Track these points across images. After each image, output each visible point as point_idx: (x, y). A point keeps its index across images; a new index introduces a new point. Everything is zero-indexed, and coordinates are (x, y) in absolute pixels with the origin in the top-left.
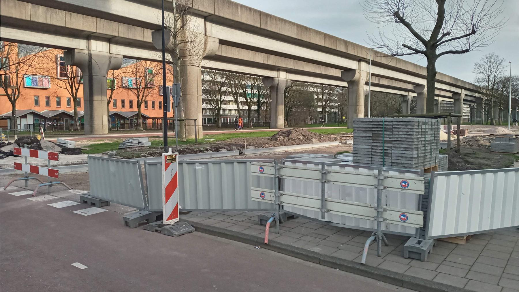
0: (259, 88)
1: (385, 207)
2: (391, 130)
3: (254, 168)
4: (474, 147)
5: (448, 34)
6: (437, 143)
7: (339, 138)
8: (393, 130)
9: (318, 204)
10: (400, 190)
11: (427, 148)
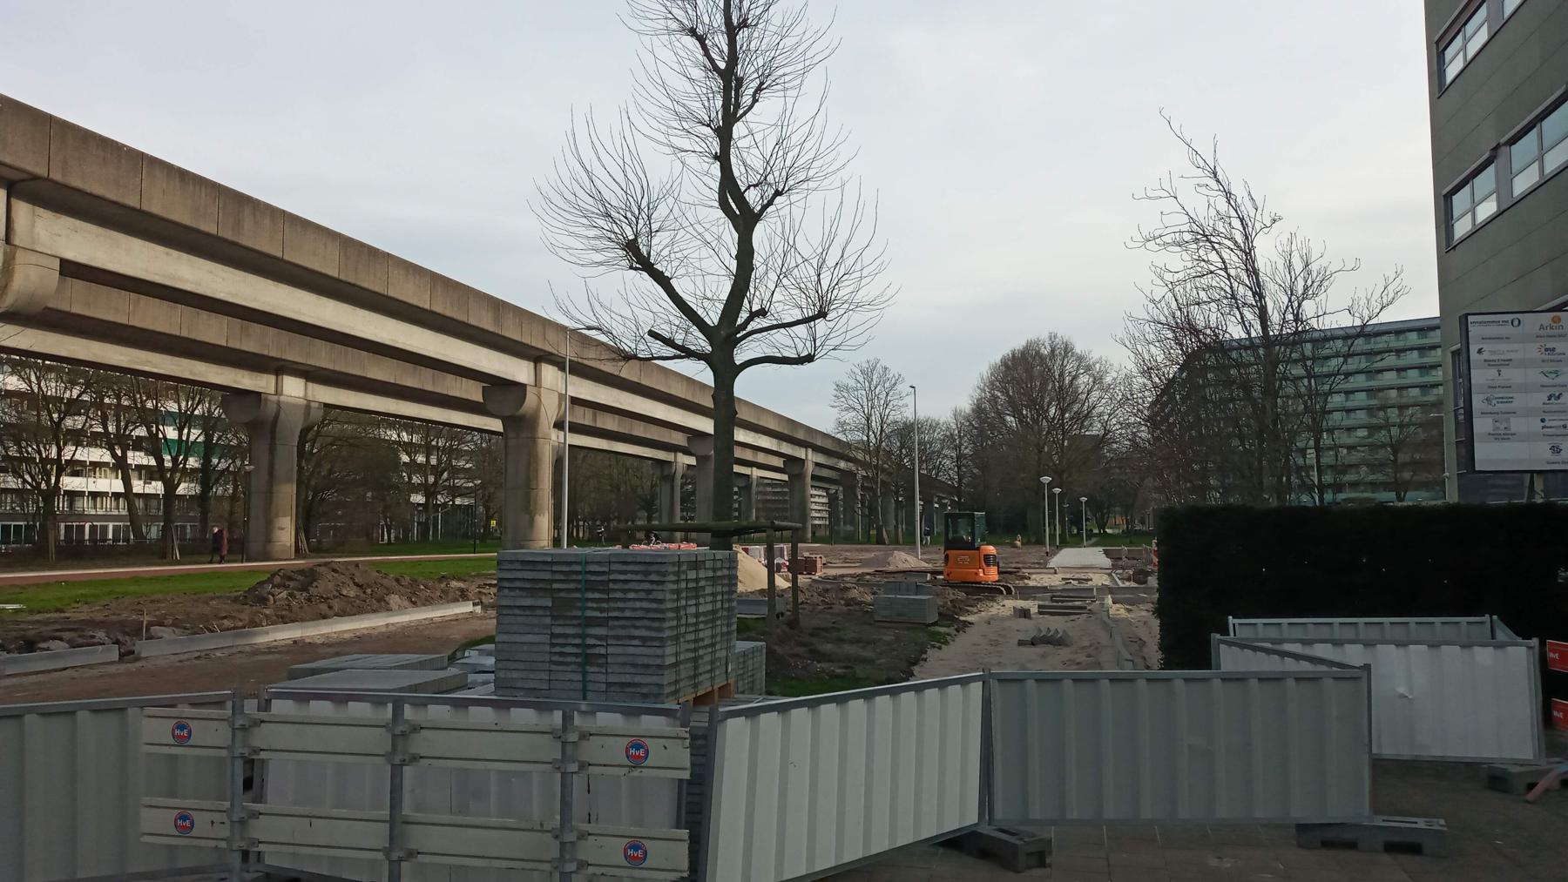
0: (207, 424)
1: (585, 827)
2: (603, 587)
3: (153, 729)
4: (837, 608)
5: (762, 313)
6: (728, 617)
7: (474, 589)
8: (611, 586)
9: (377, 835)
10: (625, 770)
11: (701, 635)
